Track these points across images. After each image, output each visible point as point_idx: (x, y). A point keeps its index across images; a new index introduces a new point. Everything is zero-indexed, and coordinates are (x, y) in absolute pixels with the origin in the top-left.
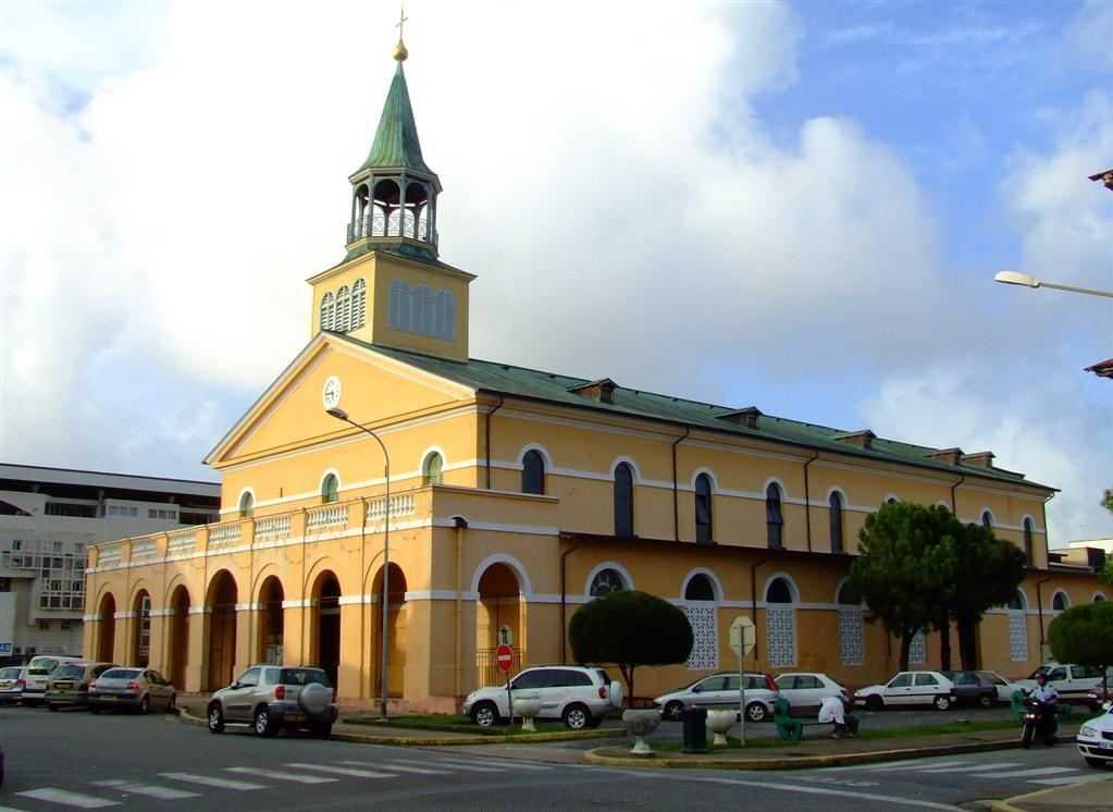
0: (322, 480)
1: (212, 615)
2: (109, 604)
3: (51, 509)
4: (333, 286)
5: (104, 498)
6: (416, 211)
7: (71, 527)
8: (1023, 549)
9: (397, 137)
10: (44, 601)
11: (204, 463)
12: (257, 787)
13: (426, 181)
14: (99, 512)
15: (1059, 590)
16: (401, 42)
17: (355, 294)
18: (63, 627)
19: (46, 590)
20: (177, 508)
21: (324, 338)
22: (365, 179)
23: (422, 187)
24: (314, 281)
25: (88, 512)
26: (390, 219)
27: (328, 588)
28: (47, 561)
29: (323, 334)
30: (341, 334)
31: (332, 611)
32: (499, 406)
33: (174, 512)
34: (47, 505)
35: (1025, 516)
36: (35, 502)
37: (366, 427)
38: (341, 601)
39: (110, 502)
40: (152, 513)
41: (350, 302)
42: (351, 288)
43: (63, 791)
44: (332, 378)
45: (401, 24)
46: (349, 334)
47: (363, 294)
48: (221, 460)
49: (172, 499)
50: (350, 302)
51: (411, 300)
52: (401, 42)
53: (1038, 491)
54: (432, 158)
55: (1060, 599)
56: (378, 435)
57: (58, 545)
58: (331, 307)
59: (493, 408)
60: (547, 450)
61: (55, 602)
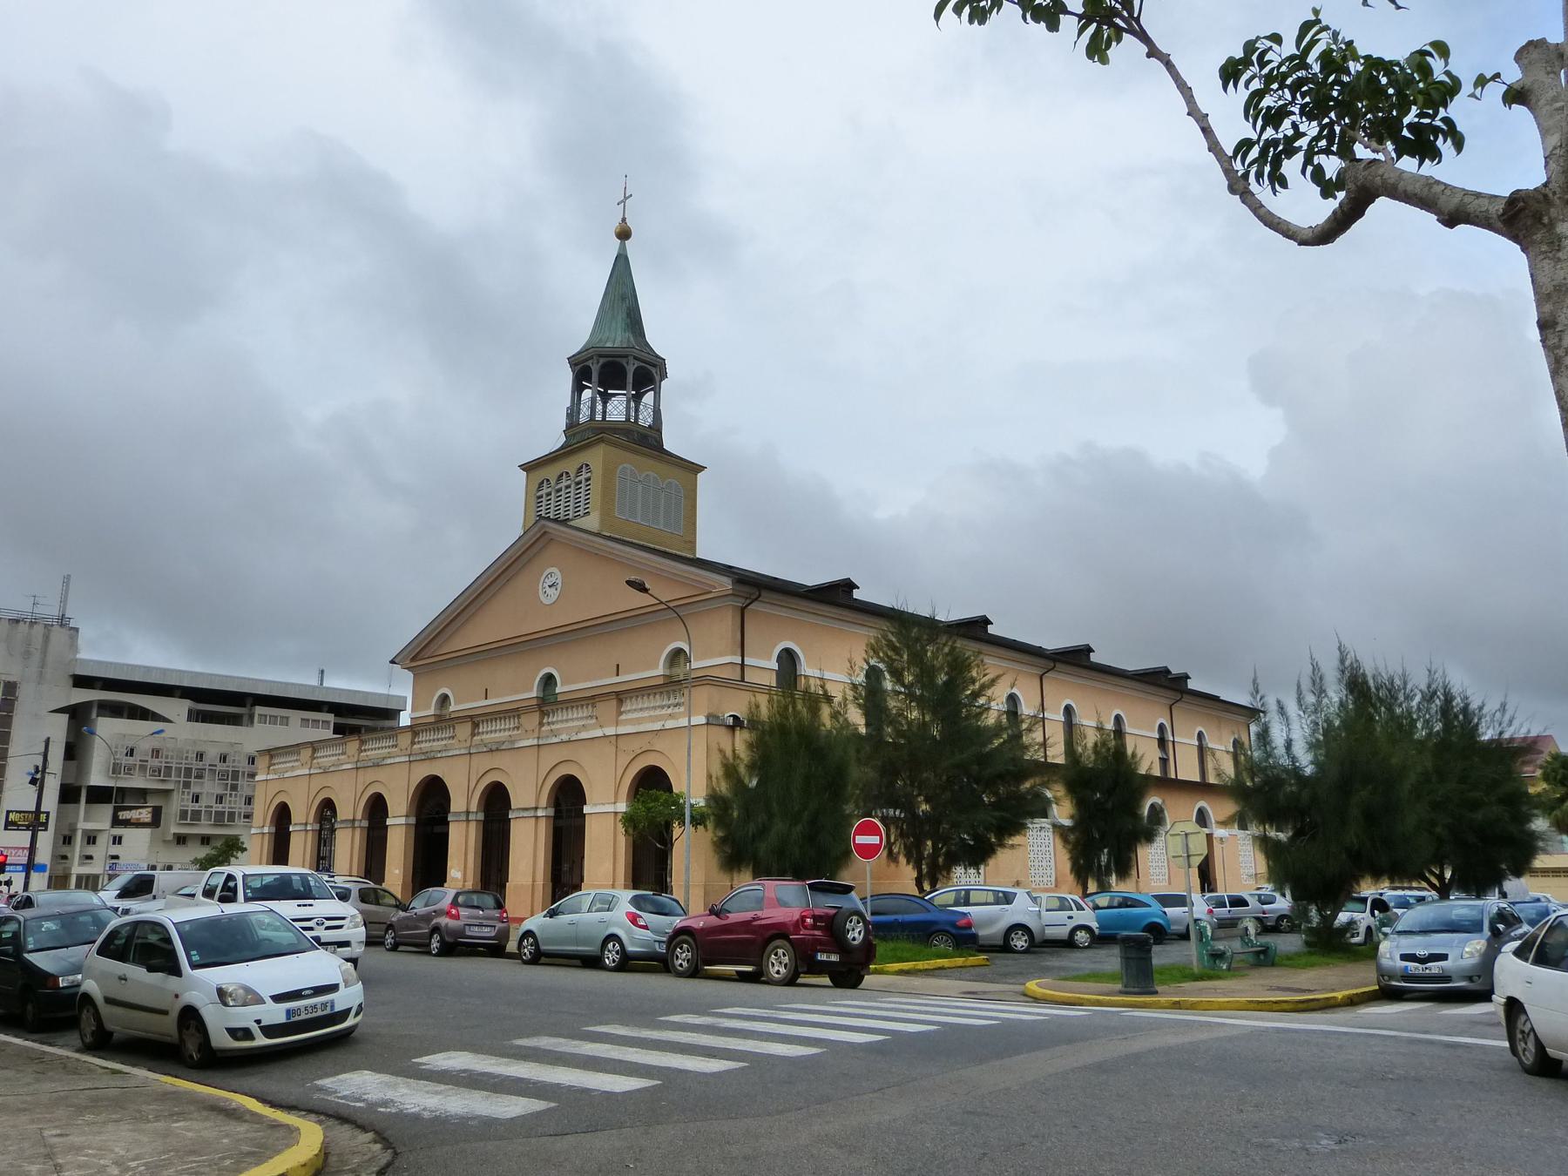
0: (538, 679)
1: (417, 825)
2: (282, 815)
3: (195, 716)
4: (551, 472)
5: (254, 705)
6: (638, 398)
7: (218, 736)
8: (224, 840)
9: (621, 316)
10: (183, 815)
11: (392, 662)
12: (936, 1027)
13: (654, 366)
14: (245, 719)
15: (1202, 804)
16: (624, 220)
17: (559, 486)
18: (203, 843)
19: (185, 803)
20: (331, 717)
21: (544, 526)
22: (587, 360)
23: (650, 373)
24: (529, 467)
25: (234, 720)
26: (609, 407)
27: (377, 808)
28: (188, 771)
29: (543, 522)
30: (565, 522)
31: (438, 829)
32: (756, 599)
33: (328, 722)
34: (190, 712)
35: (1200, 729)
36: (176, 709)
37: (671, 605)
38: (586, 809)
39: (259, 710)
40: (305, 721)
41: (572, 489)
42: (553, 482)
43: (664, 1039)
44: (554, 570)
45: (626, 198)
46: (571, 523)
47: (588, 479)
48: (413, 659)
49: (326, 708)
50: (572, 489)
51: (640, 488)
52: (624, 220)
53: (1228, 706)
54: (659, 336)
55: (1202, 812)
56: (681, 614)
57: (200, 756)
58: (549, 494)
59: (748, 601)
60: (798, 645)
61: (196, 815)
